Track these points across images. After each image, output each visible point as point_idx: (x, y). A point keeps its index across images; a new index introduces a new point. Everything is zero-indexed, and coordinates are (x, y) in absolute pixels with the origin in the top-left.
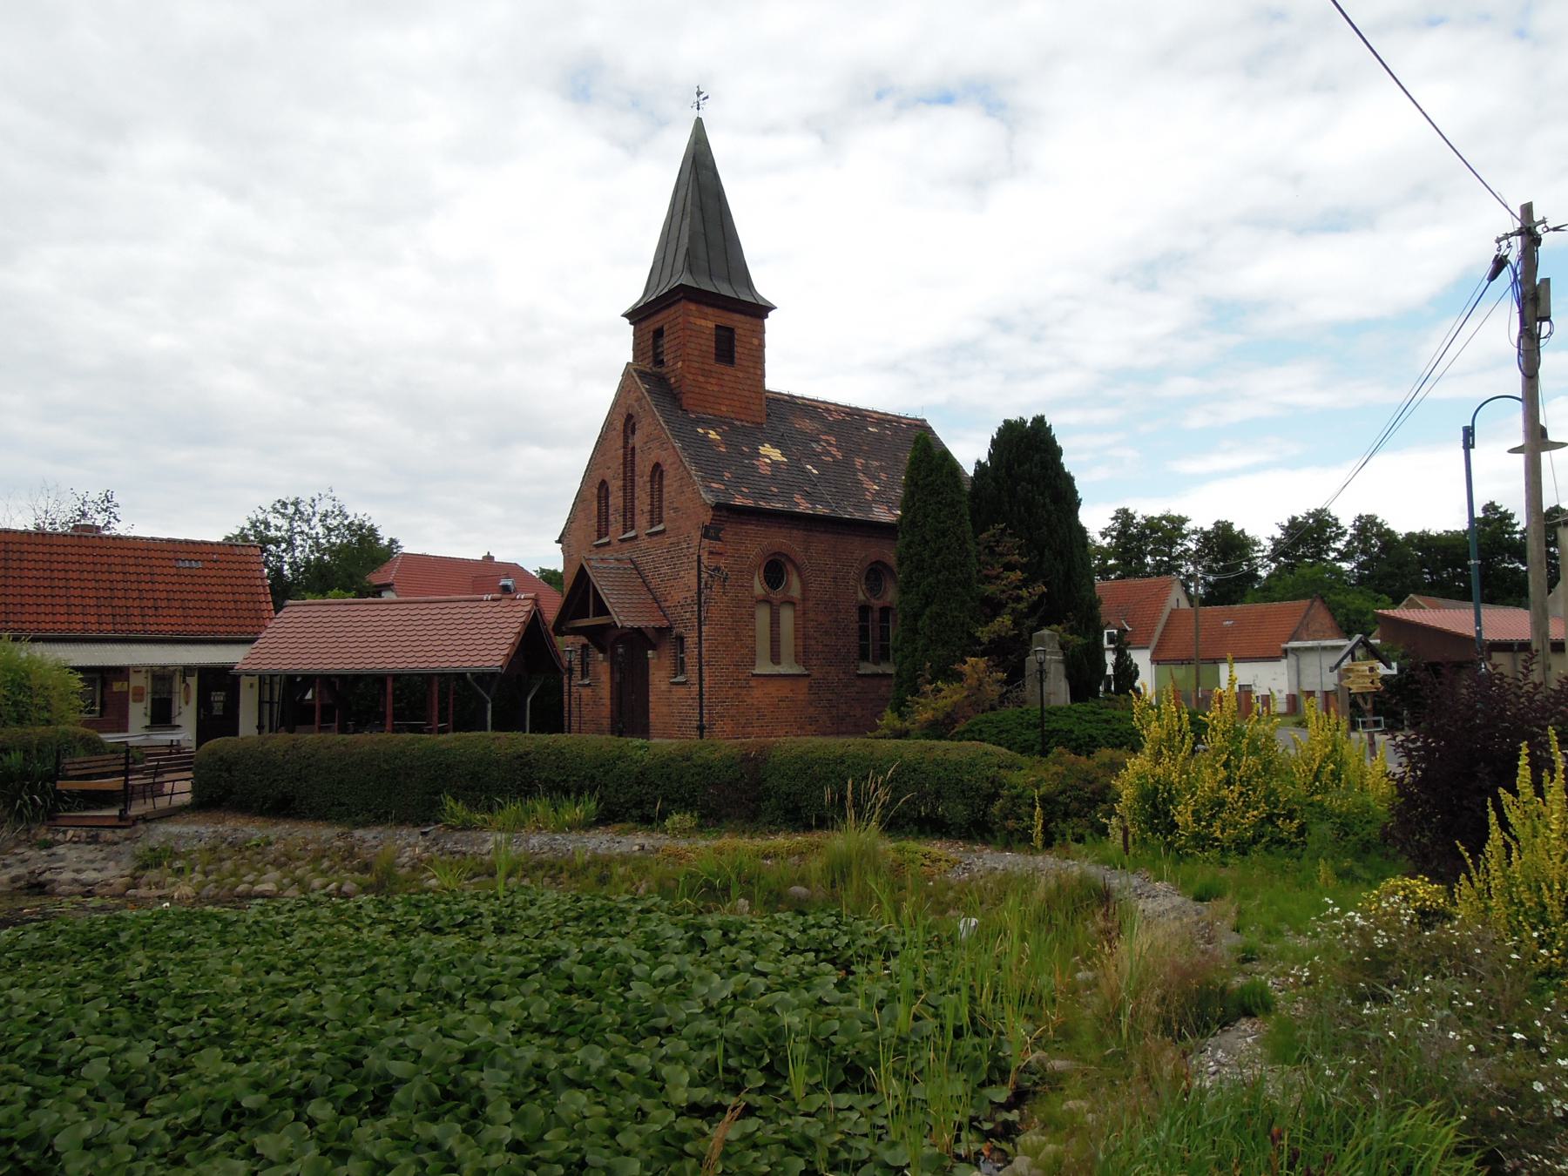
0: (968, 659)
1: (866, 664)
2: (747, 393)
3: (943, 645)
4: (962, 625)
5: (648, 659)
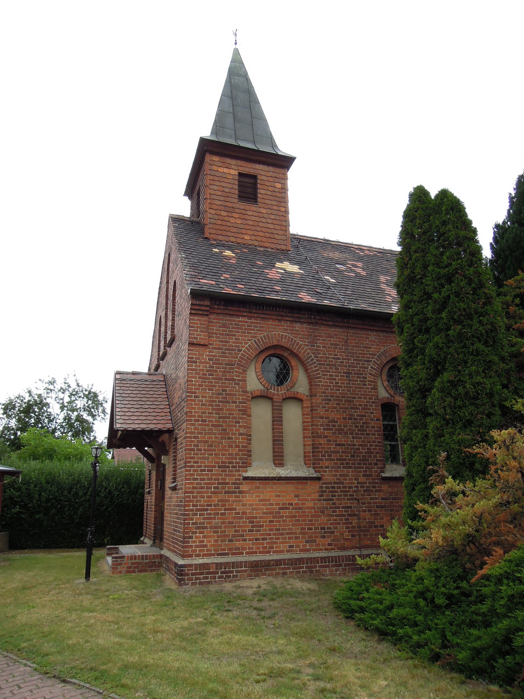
0: (495, 434)
1: (394, 466)
2: (270, 226)
3: (465, 426)
4: (491, 395)
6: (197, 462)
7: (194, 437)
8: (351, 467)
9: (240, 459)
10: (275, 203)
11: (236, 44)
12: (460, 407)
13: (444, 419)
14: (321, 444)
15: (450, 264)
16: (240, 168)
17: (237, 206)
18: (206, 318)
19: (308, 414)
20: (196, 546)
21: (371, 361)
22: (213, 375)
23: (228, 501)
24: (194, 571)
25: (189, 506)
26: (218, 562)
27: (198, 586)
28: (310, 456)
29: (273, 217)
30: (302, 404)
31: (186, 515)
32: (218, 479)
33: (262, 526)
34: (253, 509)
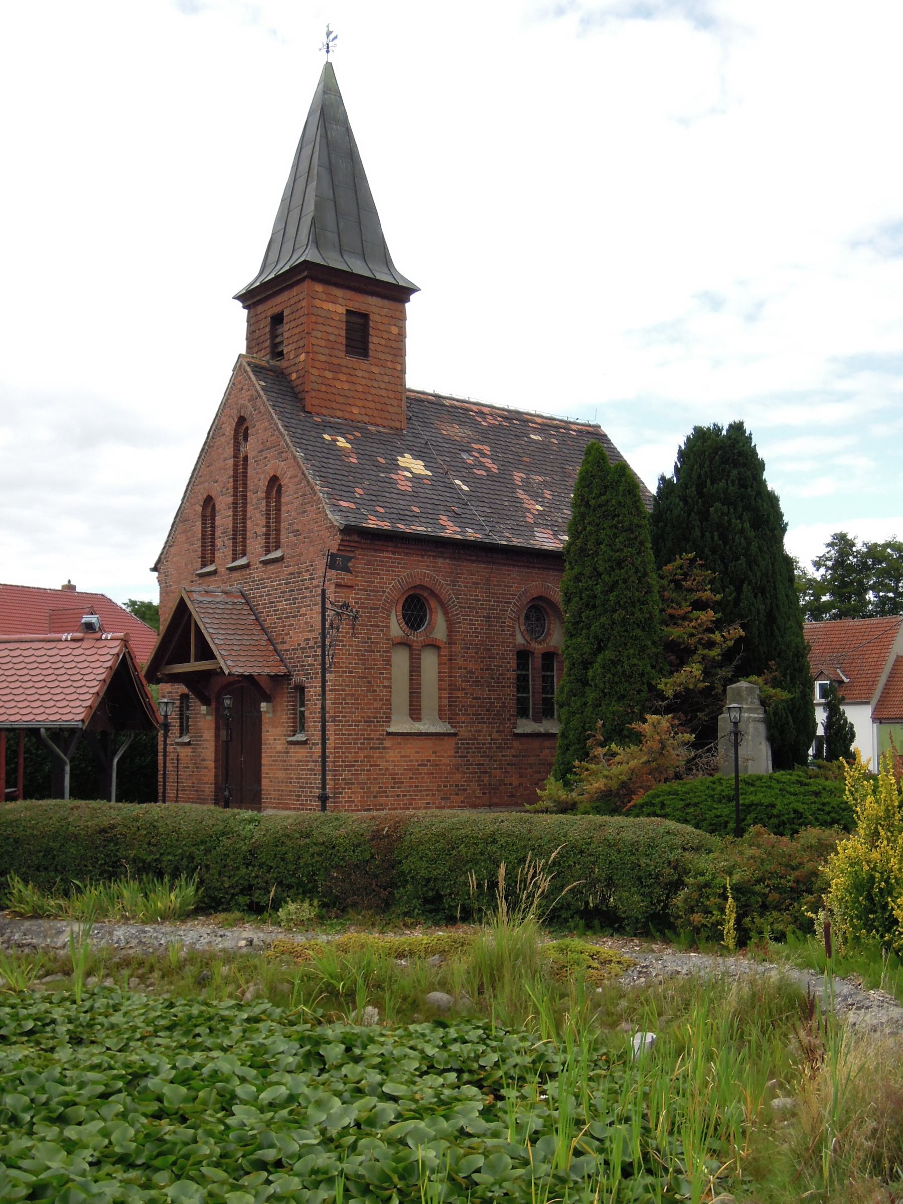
0: (648, 716)
1: (524, 721)
2: (383, 393)
3: (619, 699)
6: (345, 717)
7: (343, 690)
9: (384, 713)
12: (617, 683)
13: (603, 692)
15: (622, 550)
19: (445, 664)
20: (346, 802)
21: (511, 603)
23: (373, 757)
25: (338, 762)
29: (386, 379)
31: (335, 771)
32: (364, 735)
33: (402, 783)
34: (395, 766)
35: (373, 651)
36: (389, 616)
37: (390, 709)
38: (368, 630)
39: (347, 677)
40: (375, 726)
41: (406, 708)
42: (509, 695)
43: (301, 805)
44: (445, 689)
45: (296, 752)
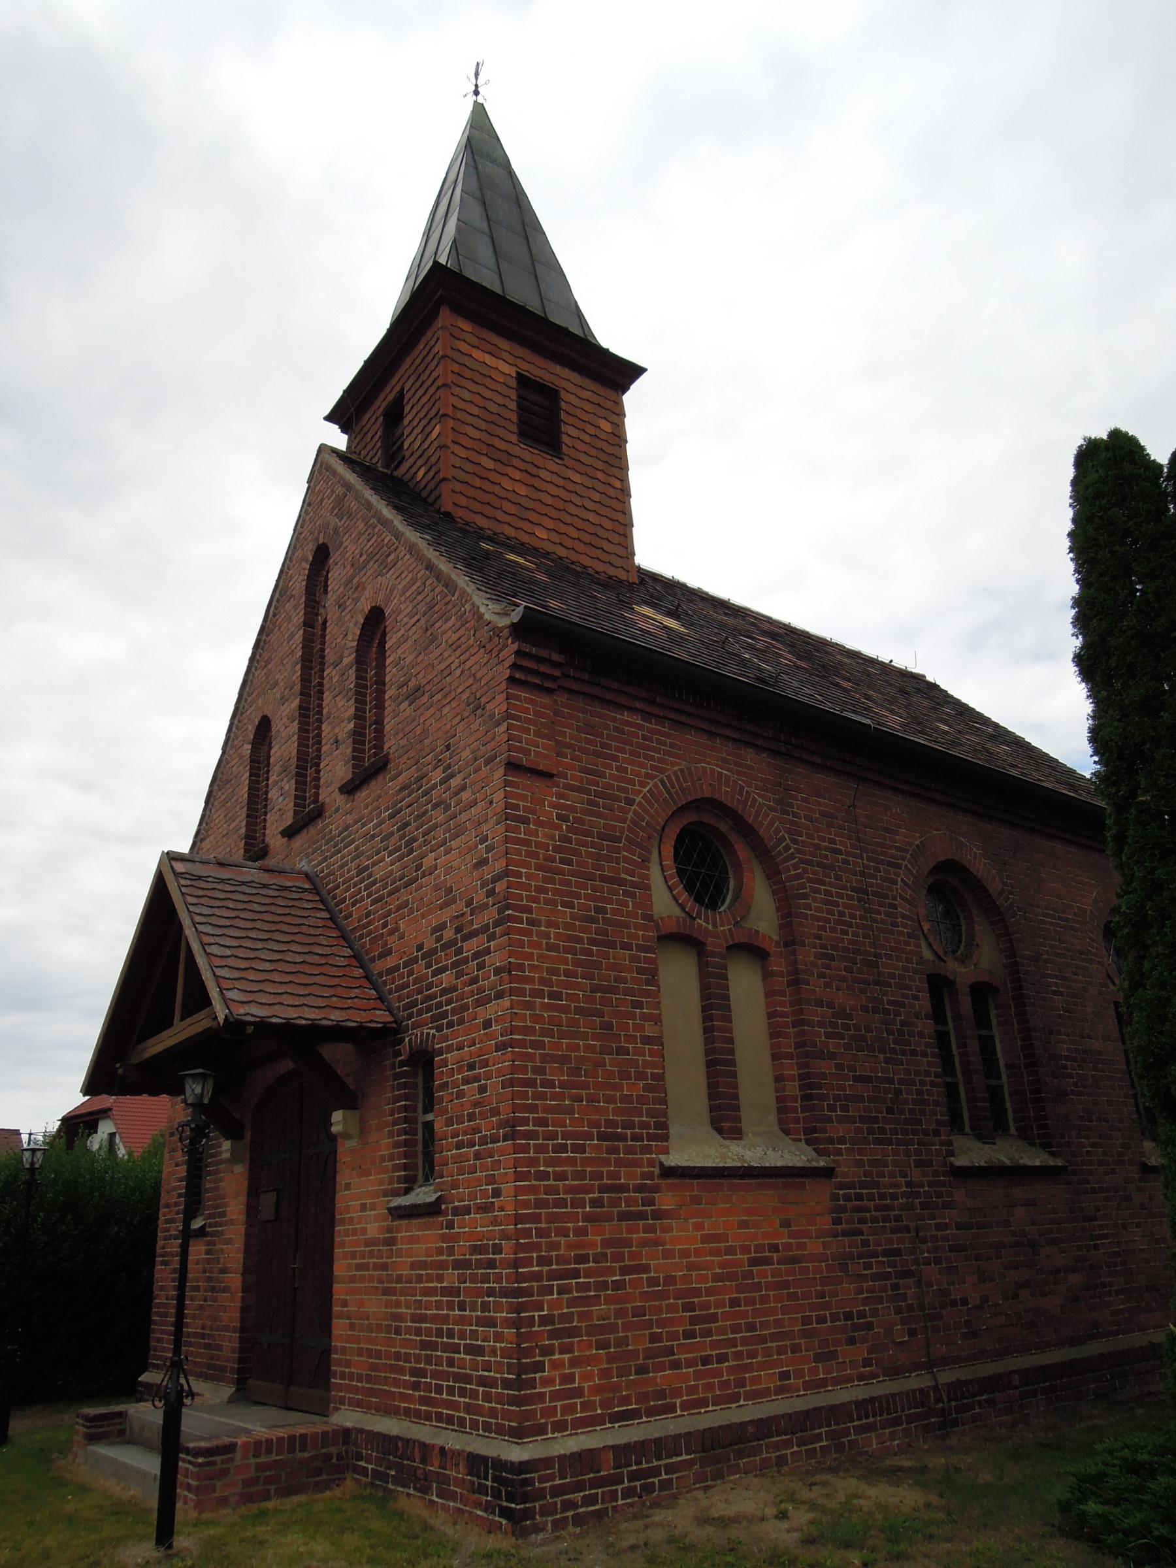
2: (591, 517)
5: (333, 1139)
6: (542, 1122)
7: (536, 1045)
8: (889, 1142)
10: (600, 465)
11: (476, 93)
14: (824, 1075)
16: (519, 362)
17: (516, 450)
18: (546, 700)
19: (783, 994)
20: (556, 1396)
21: (898, 866)
22: (570, 863)
23: (627, 1243)
24: (557, 1482)
25: (528, 1262)
26: (617, 1442)
27: (571, 1529)
28: (795, 1110)
30: (763, 969)
32: (599, 1176)
33: (713, 1318)
34: (690, 1267)
35: (612, 945)
36: (646, 860)
37: (664, 1101)
38: (594, 888)
39: (547, 1007)
40: (630, 1150)
41: (701, 1104)
42: (928, 1074)
43: (425, 1401)
44: (790, 1056)
45: (411, 1240)
